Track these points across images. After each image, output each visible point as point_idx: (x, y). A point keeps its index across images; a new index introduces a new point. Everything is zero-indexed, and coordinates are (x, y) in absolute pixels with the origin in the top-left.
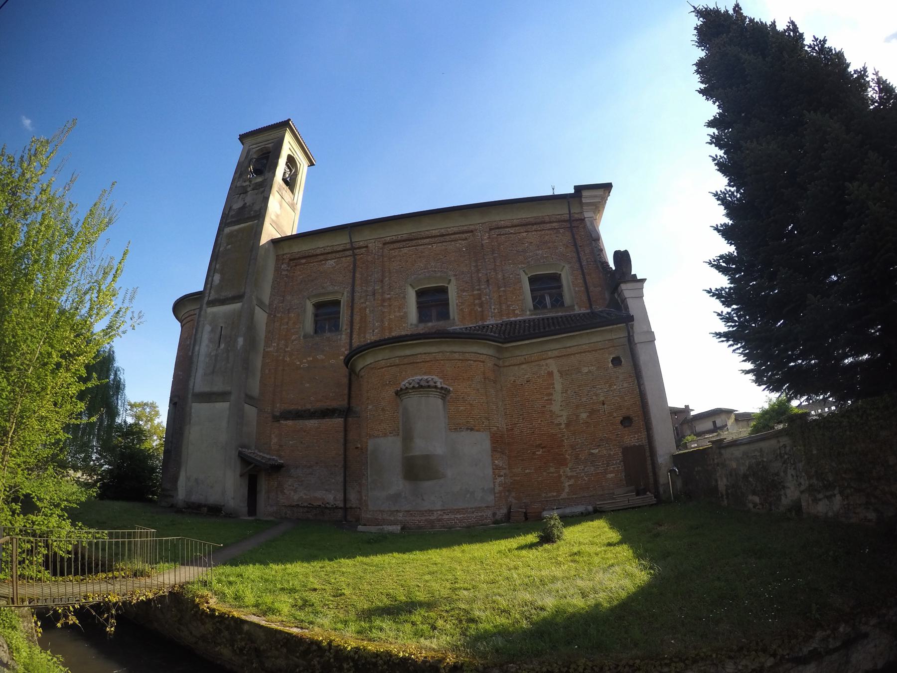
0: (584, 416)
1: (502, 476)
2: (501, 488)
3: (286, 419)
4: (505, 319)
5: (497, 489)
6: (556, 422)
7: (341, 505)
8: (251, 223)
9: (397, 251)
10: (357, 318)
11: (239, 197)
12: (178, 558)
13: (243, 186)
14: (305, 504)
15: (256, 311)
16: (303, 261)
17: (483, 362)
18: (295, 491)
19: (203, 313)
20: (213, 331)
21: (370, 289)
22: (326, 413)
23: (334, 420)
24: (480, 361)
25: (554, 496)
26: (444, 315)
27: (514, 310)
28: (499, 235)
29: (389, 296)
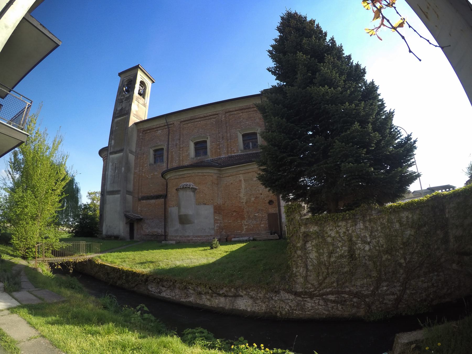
0: (253, 199)
1: (218, 223)
2: (218, 228)
3: (143, 200)
4: (230, 155)
5: (216, 228)
6: (241, 201)
7: (164, 234)
8: (125, 116)
9: (186, 125)
10: (170, 156)
11: (120, 104)
12: (89, 250)
13: (121, 99)
14: (151, 234)
15: (129, 156)
16: (149, 131)
17: (212, 176)
18: (147, 229)
19: (108, 158)
20: (112, 165)
21: (175, 143)
22: (157, 197)
23: (161, 200)
24: (211, 176)
25: (239, 232)
26: (206, 153)
27: (234, 150)
28: (230, 115)
29: (182, 146)
